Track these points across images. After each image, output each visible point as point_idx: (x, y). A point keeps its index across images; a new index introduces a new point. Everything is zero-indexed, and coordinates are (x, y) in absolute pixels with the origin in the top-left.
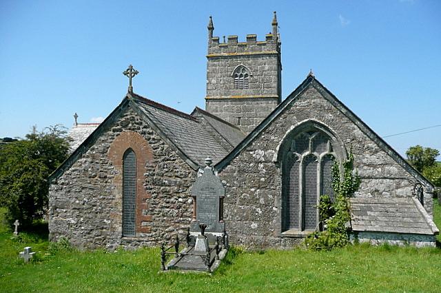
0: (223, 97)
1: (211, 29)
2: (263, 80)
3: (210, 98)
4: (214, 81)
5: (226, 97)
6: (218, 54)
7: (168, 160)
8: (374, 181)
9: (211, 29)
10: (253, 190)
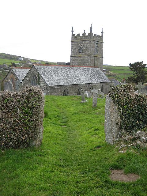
1: (72, 31)
3: (72, 56)
4: (73, 50)
9: (72, 31)
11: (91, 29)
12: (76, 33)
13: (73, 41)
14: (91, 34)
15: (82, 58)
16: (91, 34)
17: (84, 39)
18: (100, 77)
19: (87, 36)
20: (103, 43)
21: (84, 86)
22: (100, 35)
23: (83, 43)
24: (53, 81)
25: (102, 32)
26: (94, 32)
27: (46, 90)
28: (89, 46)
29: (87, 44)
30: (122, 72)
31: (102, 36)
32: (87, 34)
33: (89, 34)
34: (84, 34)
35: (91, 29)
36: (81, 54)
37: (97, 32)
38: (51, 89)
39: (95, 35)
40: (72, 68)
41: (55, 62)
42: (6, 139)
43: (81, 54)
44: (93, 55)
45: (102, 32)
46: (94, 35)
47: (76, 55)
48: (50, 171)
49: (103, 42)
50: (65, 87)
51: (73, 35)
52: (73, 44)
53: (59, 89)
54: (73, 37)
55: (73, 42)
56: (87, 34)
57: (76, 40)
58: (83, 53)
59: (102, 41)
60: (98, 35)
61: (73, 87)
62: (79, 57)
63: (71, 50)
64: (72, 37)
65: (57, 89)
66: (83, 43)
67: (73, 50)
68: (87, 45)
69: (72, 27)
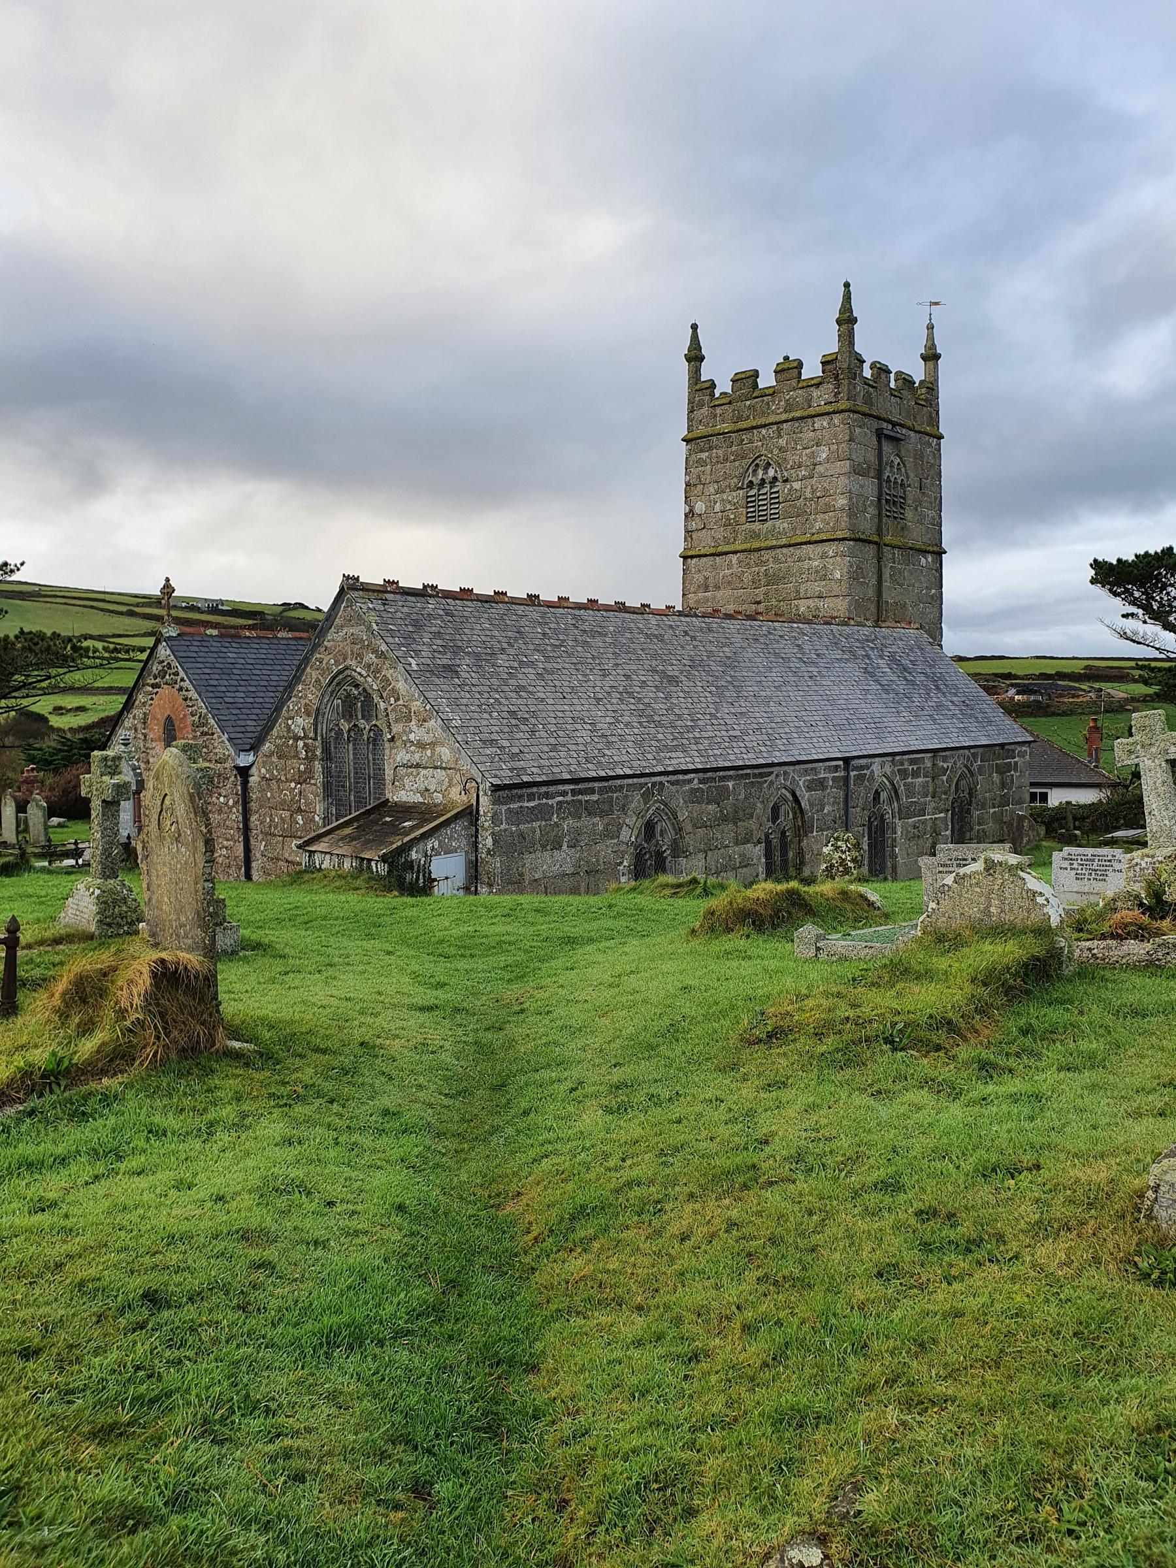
0: (720, 549)
1: (695, 357)
2: (813, 491)
4: (700, 507)
5: (726, 549)
6: (709, 431)
7: (207, 734)
8: (423, 772)
9: (695, 357)
10: (293, 785)
11: (847, 320)
12: (720, 372)
13: (702, 430)
16: (843, 366)
18: (939, 706)
20: (941, 437)
22: (918, 372)
25: (931, 357)
26: (869, 347)
27: (458, 826)
30: (1133, 664)
31: (931, 387)
32: (812, 370)
34: (789, 369)
35: (847, 320)
37: (889, 347)
38: (516, 817)
39: (881, 370)
42: (581, 747)
45: (931, 357)
46: (867, 373)
48: (535, 1160)
50: (647, 796)
51: (701, 389)
52: (701, 463)
53: (591, 810)
54: (701, 405)
55: (701, 443)
56: (812, 370)
57: (726, 427)
59: (934, 420)
60: (899, 374)
61: (719, 796)
63: (682, 509)
65: (577, 810)
69: (694, 327)
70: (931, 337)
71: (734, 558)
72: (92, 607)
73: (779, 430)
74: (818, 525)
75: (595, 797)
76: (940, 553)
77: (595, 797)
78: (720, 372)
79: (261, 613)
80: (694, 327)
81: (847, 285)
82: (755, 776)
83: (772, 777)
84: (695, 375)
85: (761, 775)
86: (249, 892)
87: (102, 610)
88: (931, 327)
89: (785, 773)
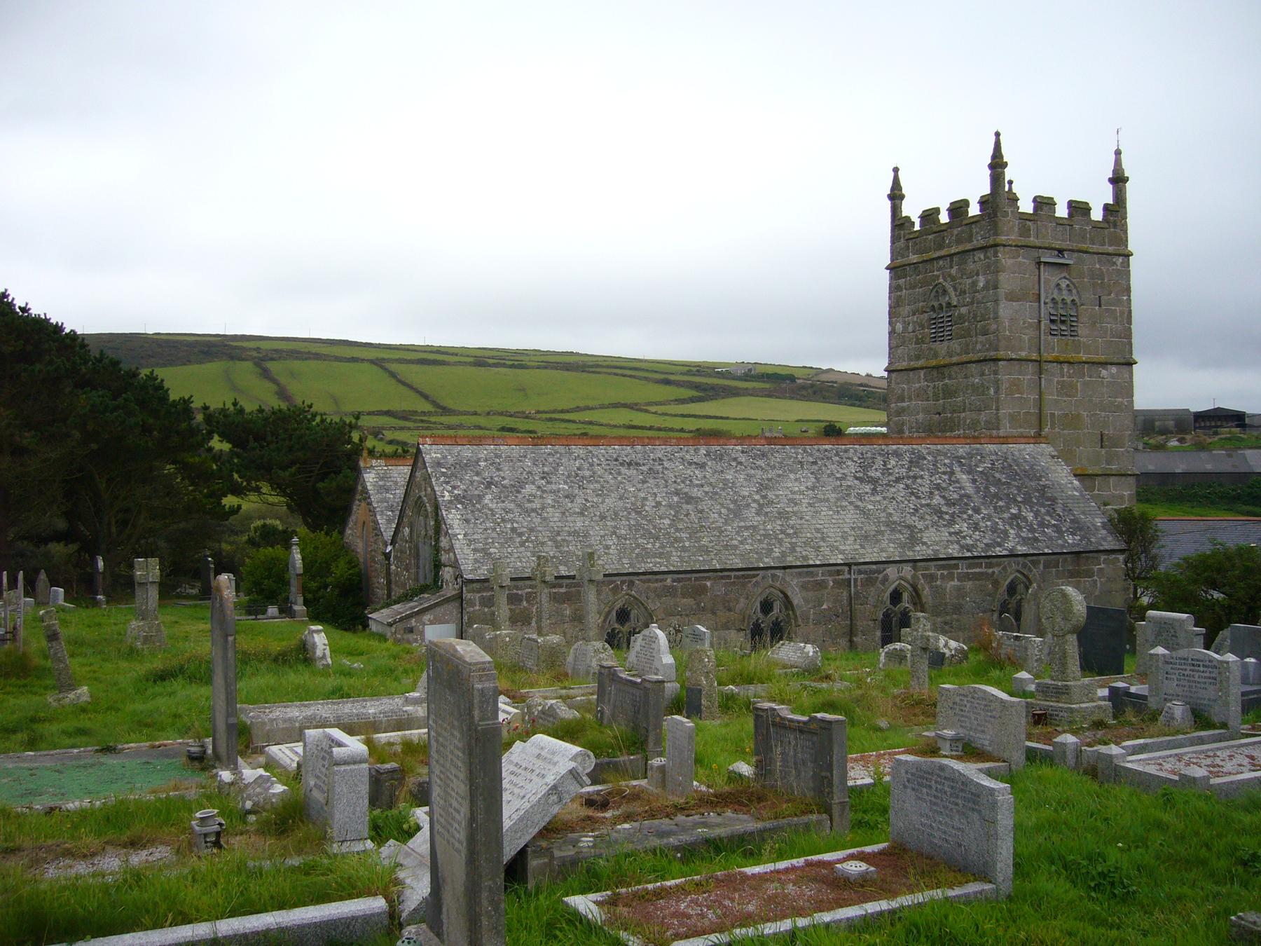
1: (896, 196)
9: (896, 196)
11: (997, 165)
13: (899, 261)
14: (999, 197)
15: (950, 378)
16: (999, 197)
17: (959, 241)
19: (976, 221)
20: (1128, 255)
21: (821, 585)
22: (1099, 198)
23: (953, 271)
24: (522, 544)
25: (1118, 180)
28: (985, 288)
29: (978, 274)
31: (1116, 210)
33: (1106, 208)
34: (958, 209)
36: (945, 350)
37: (1055, 175)
40: (764, 455)
41: (36, 310)
43: (945, 350)
44: (1023, 354)
45: (1118, 180)
47: (918, 358)
49: (1131, 247)
51: (899, 224)
58: (955, 345)
59: (1124, 241)
62: (935, 373)
64: (894, 239)
66: (953, 271)
67: (899, 327)
68: (974, 284)
69: (896, 170)
70: (1118, 163)
71: (922, 373)
72: (616, 374)
73: (952, 261)
74: (979, 347)
75: (563, 590)
76: (1130, 364)
77: (563, 590)
78: (912, 210)
79: (792, 378)
80: (896, 170)
81: (997, 134)
82: (736, 577)
83: (759, 578)
84: (896, 210)
85: (749, 577)
86: (853, 730)
87: (630, 376)
88: (1118, 153)
89: (774, 576)
